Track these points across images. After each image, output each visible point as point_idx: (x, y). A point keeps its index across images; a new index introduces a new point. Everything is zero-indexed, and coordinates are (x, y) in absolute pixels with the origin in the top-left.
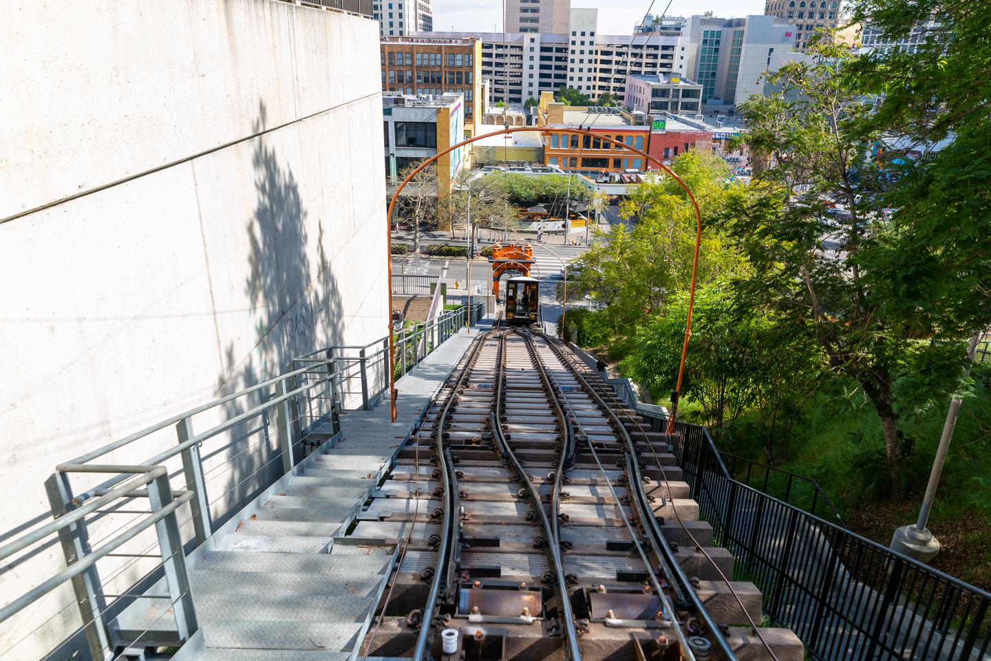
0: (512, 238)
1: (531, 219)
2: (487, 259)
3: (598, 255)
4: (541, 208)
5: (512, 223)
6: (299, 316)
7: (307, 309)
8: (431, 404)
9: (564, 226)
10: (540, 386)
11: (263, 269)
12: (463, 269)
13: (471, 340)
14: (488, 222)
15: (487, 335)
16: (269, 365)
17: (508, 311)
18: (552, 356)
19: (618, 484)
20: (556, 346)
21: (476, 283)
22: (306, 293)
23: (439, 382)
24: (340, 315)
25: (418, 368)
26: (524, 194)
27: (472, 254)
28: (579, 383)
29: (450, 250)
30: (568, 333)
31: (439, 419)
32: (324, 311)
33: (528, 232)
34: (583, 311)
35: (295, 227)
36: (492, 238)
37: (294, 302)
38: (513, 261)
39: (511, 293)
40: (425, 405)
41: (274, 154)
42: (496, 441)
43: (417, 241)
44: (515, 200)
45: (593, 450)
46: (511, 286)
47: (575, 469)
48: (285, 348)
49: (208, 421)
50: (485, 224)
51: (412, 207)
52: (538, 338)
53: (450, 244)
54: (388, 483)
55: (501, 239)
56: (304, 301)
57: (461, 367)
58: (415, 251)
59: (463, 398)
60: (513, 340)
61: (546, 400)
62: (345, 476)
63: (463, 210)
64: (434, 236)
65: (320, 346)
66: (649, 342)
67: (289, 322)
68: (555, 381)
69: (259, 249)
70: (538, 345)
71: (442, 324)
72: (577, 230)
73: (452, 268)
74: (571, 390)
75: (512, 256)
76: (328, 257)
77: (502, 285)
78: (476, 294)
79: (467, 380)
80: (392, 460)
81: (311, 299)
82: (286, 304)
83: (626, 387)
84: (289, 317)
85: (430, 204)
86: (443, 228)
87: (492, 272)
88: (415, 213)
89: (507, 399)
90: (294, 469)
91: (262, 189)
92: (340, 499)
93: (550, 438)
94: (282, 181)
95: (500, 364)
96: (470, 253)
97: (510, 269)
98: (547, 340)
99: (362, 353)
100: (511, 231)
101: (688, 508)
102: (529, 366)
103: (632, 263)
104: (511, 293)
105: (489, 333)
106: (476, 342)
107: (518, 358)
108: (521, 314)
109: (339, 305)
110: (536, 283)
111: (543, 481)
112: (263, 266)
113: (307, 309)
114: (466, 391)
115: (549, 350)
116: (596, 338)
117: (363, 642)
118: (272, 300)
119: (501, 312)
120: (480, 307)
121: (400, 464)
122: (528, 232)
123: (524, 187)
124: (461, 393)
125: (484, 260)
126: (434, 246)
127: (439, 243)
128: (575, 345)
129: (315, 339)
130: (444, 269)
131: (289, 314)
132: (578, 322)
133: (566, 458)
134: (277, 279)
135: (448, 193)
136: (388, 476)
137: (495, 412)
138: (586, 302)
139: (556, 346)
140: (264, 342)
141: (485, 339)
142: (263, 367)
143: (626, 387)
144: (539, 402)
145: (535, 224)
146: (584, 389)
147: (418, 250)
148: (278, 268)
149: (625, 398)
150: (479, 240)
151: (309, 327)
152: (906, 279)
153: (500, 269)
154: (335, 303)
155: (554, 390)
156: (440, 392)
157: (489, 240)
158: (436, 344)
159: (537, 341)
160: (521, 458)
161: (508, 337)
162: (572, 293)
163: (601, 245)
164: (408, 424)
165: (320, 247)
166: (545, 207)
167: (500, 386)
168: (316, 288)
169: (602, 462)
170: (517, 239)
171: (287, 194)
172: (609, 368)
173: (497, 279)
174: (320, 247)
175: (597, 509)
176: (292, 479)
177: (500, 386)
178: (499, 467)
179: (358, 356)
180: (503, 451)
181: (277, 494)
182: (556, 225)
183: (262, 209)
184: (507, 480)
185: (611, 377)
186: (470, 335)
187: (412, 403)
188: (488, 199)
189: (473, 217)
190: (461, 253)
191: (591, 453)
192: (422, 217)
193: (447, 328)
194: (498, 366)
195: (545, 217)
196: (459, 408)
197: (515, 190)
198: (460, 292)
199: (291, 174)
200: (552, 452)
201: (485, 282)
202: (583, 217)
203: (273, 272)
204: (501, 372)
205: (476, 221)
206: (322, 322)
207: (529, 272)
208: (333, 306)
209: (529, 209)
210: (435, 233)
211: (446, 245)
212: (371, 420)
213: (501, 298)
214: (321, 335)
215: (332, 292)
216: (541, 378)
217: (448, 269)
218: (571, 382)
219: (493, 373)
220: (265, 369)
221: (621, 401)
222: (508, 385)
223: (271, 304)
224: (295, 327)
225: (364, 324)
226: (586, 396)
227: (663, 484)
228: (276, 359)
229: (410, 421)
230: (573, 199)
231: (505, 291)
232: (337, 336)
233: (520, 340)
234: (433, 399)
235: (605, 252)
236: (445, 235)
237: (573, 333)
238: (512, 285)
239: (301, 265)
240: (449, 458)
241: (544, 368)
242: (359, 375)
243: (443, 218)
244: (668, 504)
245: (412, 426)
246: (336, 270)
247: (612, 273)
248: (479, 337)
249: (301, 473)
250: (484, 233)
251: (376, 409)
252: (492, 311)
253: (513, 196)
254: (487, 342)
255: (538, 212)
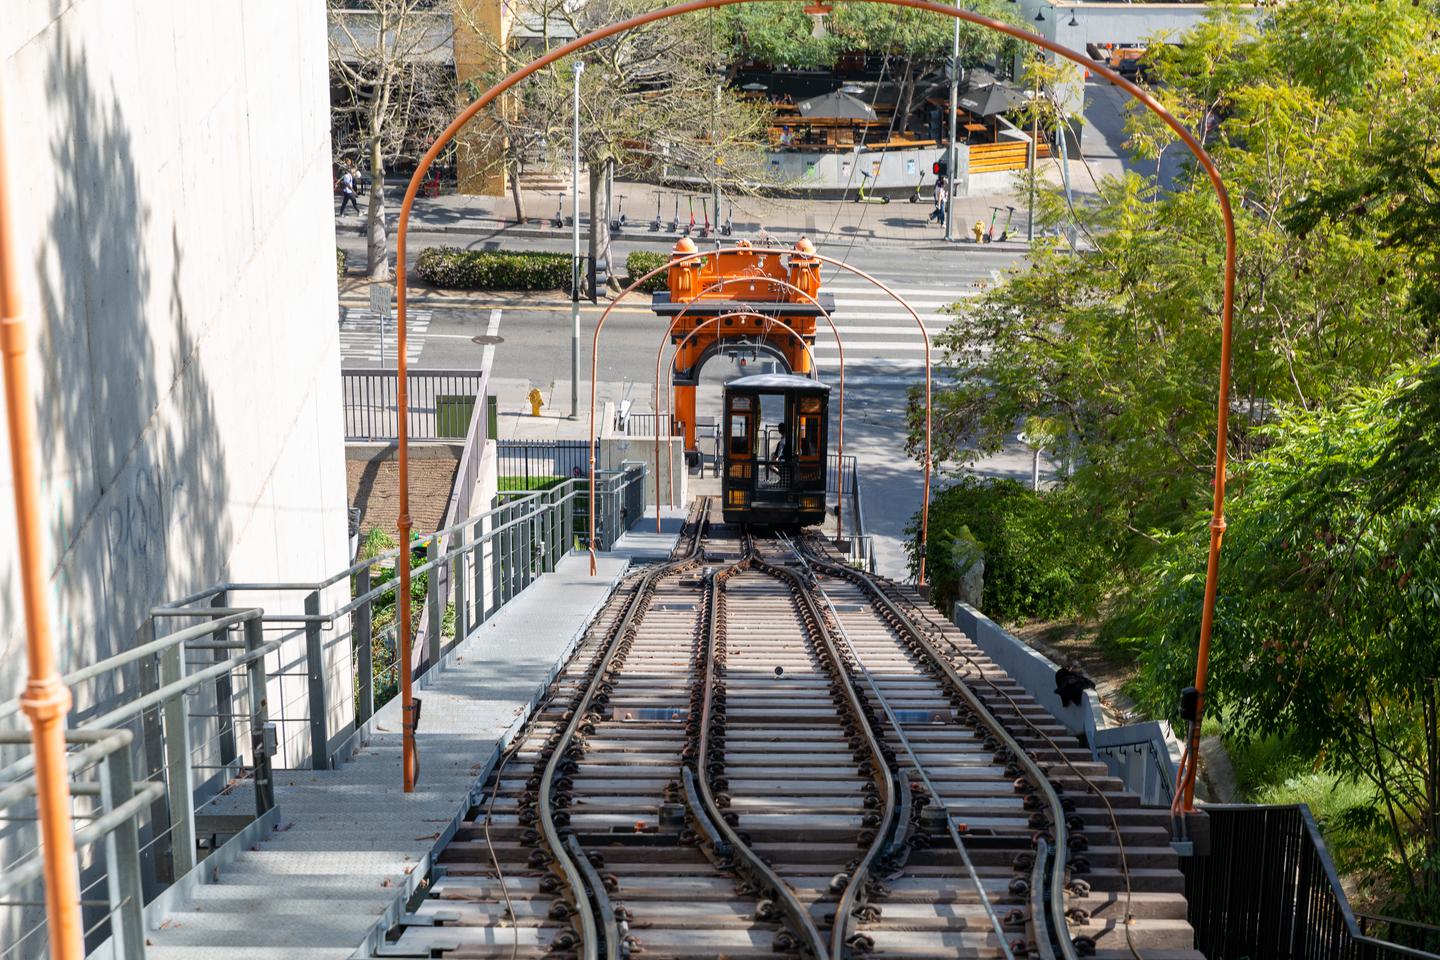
0: (737, 218)
1: (814, 142)
2: (648, 300)
3: (1052, 286)
4: (853, 102)
5: (740, 159)
6: (133, 500)
7: (149, 482)
8: (504, 759)
9: (941, 168)
10: (833, 712)
11: (64, 372)
12: (559, 340)
13: (605, 592)
14: (649, 161)
15: (656, 576)
16: (75, 633)
17: (729, 484)
18: (883, 635)
19: (1007, 897)
20: (898, 608)
21: (606, 391)
22: (147, 434)
23: (517, 706)
24: (220, 499)
25: (443, 670)
26: (786, 50)
27: (593, 283)
28: (954, 704)
29: (505, 269)
30: (948, 569)
31: (534, 787)
32: (185, 487)
33: (804, 194)
34: (1009, 489)
35: (125, 249)
36: (666, 218)
37: (123, 460)
38: (745, 311)
39: (738, 430)
40: (490, 755)
41: (84, 61)
42: (698, 825)
43: (380, 233)
44: (755, 73)
45: (957, 839)
46: (739, 404)
47: (904, 876)
48: (106, 586)
49: (337, 598)
50: (640, 166)
51: (358, 106)
52: (839, 584)
53: (507, 244)
54: (428, 905)
55: (700, 223)
56: (143, 456)
57: (579, 668)
58: (368, 272)
59: (595, 745)
60: (749, 593)
61: (855, 771)
62: (323, 884)
63: (555, 114)
64: (442, 215)
65: (179, 591)
66: (1188, 577)
67: (114, 515)
68: (876, 692)
69: (57, 319)
70: (832, 603)
71: (505, 535)
72: (986, 180)
73: (513, 338)
74: (925, 721)
75: (741, 291)
76: (193, 328)
77: (709, 397)
78: (609, 433)
79: (604, 699)
80: (431, 862)
81: (157, 453)
82: (107, 466)
83: (1153, 752)
84: (114, 503)
85: (429, 95)
86: (478, 186)
87: (671, 352)
88: (368, 129)
89: (728, 757)
90: (198, 869)
91: (63, 159)
92: (332, 917)
93: (853, 823)
94: (97, 132)
95: (704, 657)
96: (582, 279)
97: (735, 336)
98: (869, 590)
99: (312, 604)
100: (739, 192)
101: (1167, 934)
102: (800, 663)
103: (1167, 311)
104: (738, 430)
105: (665, 572)
106: (620, 601)
107: (764, 639)
108: (777, 500)
109: (218, 469)
110: (821, 394)
111: (819, 896)
112: (64, 365)
113: (149, 482)
114: (602, 727)
115: (873, 619)
116: (1052, 586)
117: (550, 847)
118: (80, 454)
119: (706, 502)
120: (635, 478)
121: (449, 874)
122: (804, 194)
123: (788, 22)
124: (589, 731)
125: (637, 304)
126: (446, 252)
127: (461, 243)
128: (977, 614)
129: (168, 565)
130: (485, 340)
131: (114, 495)
132: (988, 531)
133: (881, 850)
134: (91, 398)
135: (496, 52)
136: (422, 894)
137: (694, 769)
138: (1024, 460)
139: (898, 608)
140: (65, 567)
141: (651, 589)
142: (64, 634)
143: (1153, 752)
144: (830, 752)
145: (829, 161)
146: (967, 718)
147: (383, 272)
148: (93, 369)
149: (1150, 793)
150: (615, 229)
151: (155, 532)
152: (1313, 406)
153: (699, 340)
154: (211, 462)
155: (873, 721)
156: (523, 729)
157: (655, 226)
158: (488, 604)
159: (830, 594)
160: (770, 858)
161: (732, 582)
162: (963, 425)
163: (1071, 244)
164: (453, 795)
165: (177, 301)
166: (866, 98)
167: (708, 716)
168: (169, 418)
169: (975, 864)
170: (769, 225)
171: (110, 162)
172: (1102, 692)
173: (687, 377)
174: (177, 301)
175: (944, 938)
176: (193, 882)
177: (708, 716)
178: (708, 875)
179: (300, 610)
180: (717, 839)
181: (175, 909)
182: (909, 165)
183: (62, 212)
184: (731, 895)
185: (1106, 724)
186: (596, 579)
187: (449, 751)
188: (645, 70)
189: (589, 141)
190: (548, 278)
191: (954, 846)
192: (398, 145)
193: (520, 558)
194: (700, 665)
195: (875, 136)
196: (586, 766)
197: (750, 33)
198: (548, 428)
199: (117, 108)
200: (851, 847)
201: (644, 390)
202: (1015, 132)
203: (81, 381)
204: (710, 677)
205: (604, 155)
206: (182, 518)
207: (810, 349)
208: (206, 473)
209: (806, 106)
210: (450, 202)
211: (491, 248)
212: (343, 788)
213: (707, 446)
214: (180, 559)
215: (203, 430)
216: (837, 693)
217: (498, 340)
218: (931, 697)
219: (684, 682)
220: (69, 640)
221: (1134, 803)
222: (730, 712)
223: (78, 465)
224: (125, 533)
225: (286, 529)
226: (970, 734)
227: (1122, 897)
228: (89, 619)
229: (454, 789)
230: (973, 63)
231: (719, 420)
232: (213, 558)
233: (774, 592)
234: (508, 746)
235: (1079, 274)
236: (484, 211)
237: (968, 567)
238: (742, 400)
239: (136, 356)
240: (584, 861)
241: (848, 667)
242: (304, 667)
243: (477, 145)
244: (1119, 927)
245: (461, 800)
246: (212, 368)
247: (1089, 355)
248: (628, 585)
249: (212, 878)
250: (635, 200)
251: (348, 767)
252: (673, 498)
253: (742, 57)
254: (656, 600)
255: (844, 114)
